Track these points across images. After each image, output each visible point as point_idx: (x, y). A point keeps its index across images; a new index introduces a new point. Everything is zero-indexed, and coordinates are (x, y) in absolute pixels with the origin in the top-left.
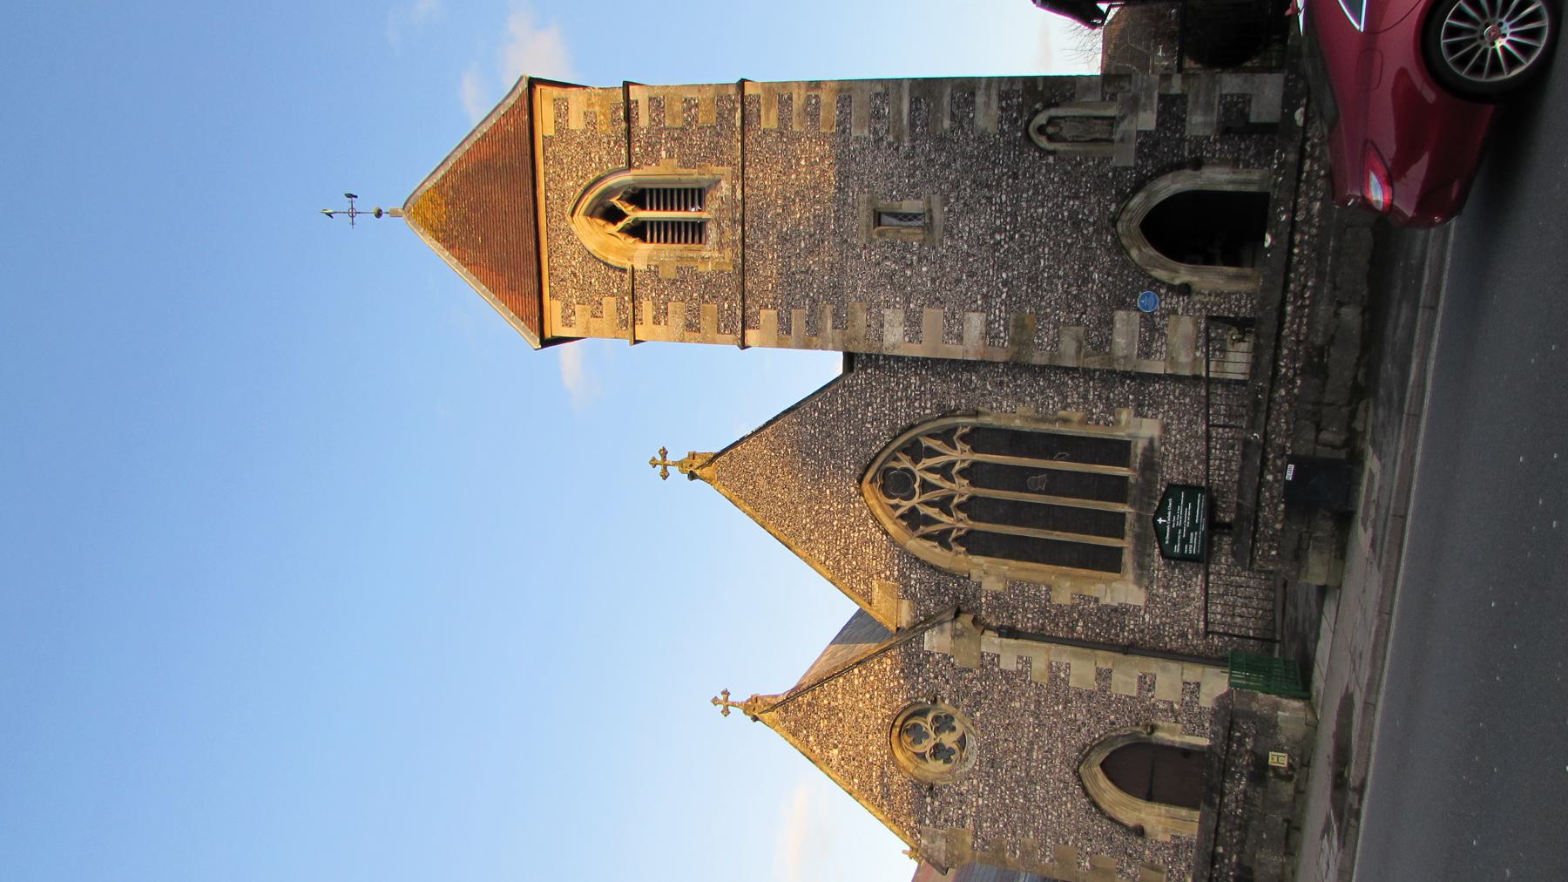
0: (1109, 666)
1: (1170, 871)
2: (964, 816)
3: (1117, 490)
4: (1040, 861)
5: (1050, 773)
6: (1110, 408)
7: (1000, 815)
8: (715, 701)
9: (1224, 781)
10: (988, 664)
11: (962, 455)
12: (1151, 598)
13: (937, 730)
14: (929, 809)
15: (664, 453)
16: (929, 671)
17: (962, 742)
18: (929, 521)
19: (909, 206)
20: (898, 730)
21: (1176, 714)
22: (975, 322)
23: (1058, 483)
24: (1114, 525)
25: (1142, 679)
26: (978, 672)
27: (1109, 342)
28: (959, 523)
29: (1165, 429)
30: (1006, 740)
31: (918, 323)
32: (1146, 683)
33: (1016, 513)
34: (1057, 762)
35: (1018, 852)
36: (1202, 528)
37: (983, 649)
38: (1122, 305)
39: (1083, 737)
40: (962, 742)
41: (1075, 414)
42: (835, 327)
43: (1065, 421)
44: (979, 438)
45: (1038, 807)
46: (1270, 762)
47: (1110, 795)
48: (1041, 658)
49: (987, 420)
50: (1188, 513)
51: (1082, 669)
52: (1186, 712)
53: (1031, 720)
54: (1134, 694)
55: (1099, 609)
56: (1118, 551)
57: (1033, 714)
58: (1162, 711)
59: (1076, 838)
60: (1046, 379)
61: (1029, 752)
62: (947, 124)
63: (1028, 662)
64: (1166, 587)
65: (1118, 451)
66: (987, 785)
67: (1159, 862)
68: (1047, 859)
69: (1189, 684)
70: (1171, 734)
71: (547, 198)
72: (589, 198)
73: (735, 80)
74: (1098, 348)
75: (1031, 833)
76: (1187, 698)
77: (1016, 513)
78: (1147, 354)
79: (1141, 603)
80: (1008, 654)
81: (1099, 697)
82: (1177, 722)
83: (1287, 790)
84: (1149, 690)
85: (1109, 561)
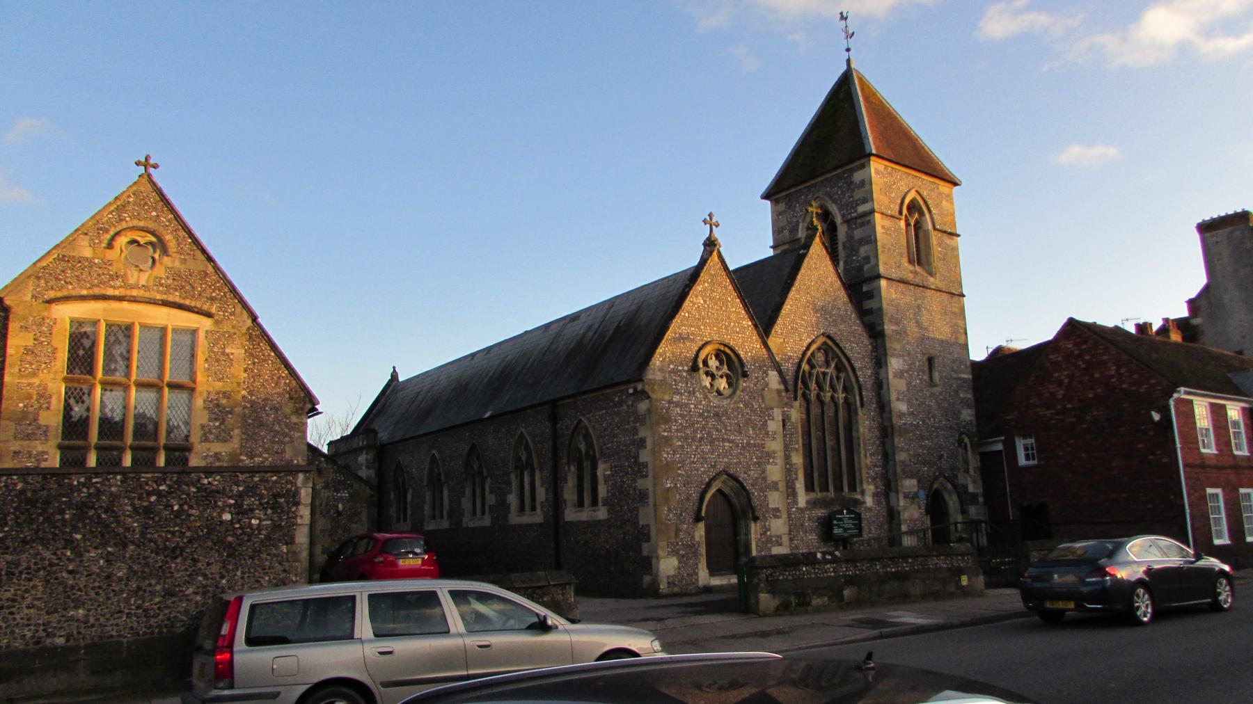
0: (781, 489)
1: (678, 544)
2: (681, 394)
3: (839, 488)
4: (664, 451)
5: (719, 456)
7: (687, 420)
8: (710, 215)
9: (943, 555)
10: (766, 413)
12: (802, 510)
14: (680, 368)
15: (155, 166)
16: (758, 373)
19: (936, 375)
20: (722, 349)
24: (825, 488)
25: (777, 510)
26: (763, 406)
27: (907, 477)
29: (870, 509)
34: (726, 460)
35: (666, 434)
36: (846, 535)
37: (775, 409)
38: (919, 482)
39: (742, 477)
41: (868, 461)
42: (892, 330)
43: (866, 456)
45: (697, 448)
46: (962, 576)
49: (860, 412)
50: (850, 526)
52: (768, 541)
53: (745, 441)
54: (770, 506)
55: (793, 480)
56: (827, 490)
57: (748, 444)
58: (765, 525)
59: (684, 475)
60: (879, 444)
61: (729, 441)
62: (962, 395)
63: (774, 438)
64: (809, 519)
66: (703, 412)
67: (682, 535)
68: (665, 455)
69: (781, 539)
70: (755, 529)
71: (899, 170)
72: (921, 202)
73: (964, 293)
74: (904, 472)
75: (680, 443)
76: (774, 539)
78: (906, 496)
82: (761, 534)
83: (952, 588)
84: (773, 515)
85: (809, 487)
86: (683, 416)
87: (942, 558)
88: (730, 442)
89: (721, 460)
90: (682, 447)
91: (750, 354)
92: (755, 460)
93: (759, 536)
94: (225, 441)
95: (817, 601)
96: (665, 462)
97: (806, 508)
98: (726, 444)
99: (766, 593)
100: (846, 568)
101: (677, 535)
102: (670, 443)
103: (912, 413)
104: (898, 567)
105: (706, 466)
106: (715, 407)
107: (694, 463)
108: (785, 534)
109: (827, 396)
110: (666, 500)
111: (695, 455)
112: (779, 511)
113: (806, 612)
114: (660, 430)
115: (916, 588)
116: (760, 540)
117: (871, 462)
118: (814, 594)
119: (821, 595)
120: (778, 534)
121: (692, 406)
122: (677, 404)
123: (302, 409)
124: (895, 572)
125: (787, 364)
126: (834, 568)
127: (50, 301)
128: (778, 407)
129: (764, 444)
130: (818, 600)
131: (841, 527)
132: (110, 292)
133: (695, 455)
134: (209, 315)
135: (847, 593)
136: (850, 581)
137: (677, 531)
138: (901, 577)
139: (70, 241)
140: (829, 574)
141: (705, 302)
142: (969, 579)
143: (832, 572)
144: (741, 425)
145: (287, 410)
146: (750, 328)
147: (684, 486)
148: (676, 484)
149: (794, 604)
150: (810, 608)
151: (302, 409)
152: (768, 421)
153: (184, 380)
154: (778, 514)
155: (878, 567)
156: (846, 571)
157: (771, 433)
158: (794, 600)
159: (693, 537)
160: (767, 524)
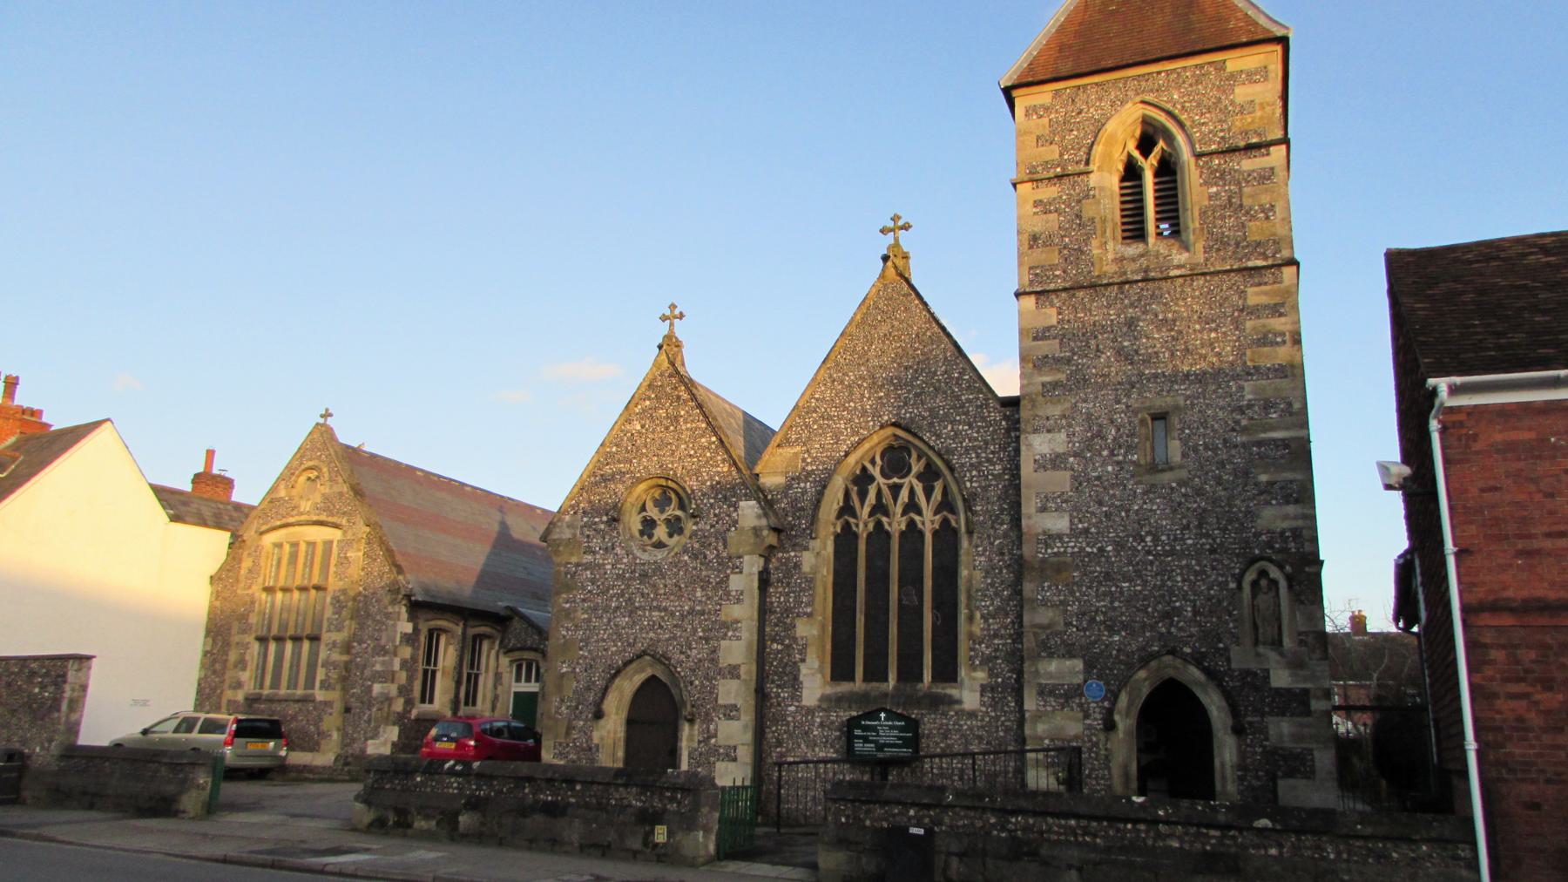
0: (743, 677)
1: (568, 745)
2: (594, 553)
3: (910, 672)
4: (562, 626)
6: (987, 661)
8: (673, 307)
10: (730, 564)
11: (928, 521)
12: (810, 711)
13: (668, 521)
14: (597, 520)
17: (660, 545)
18: (863, 495)
21: (706, 741)
22: (1059, 523)
23: (911, 616)
24: (876, 672)
25: (734, 707)
28: (863, 524)
29: (972, 715)
30: (665, 586)
31: (1055, 467)
32: (731, 712)
33: (878, 579)
34: (652, 635)
35: (568, 605)
36: (880, 755)
37: (746, 558)
40: (660, 545)
41: (978, 627)
44: (947, 537)
45: (609, 621)
47: (628, 685)
48: (744, 612)
49: (965, 543)
51: (737, 651)
53: (686, 608)
55: (795, 663)
58: (708, 728)
59: (586, 658)
63: (739, 601)
64: (822, 725)
65: (947, 671)
68: (564, 633)
69: (735, 751)
70: (688, 738)
73: (1297, 256)
75: (586, 616)
76: (721, 751)
77: (878, 579)
79: (804, 703)
80: (744, 581)
81: (715, 670)
82: (700, 742)
83: (636, 843)
84: (725, 715)
85: (841, 669)
86: (593, 581)
87: (634, 790)
88: (660, 610)
89: (644, 635)
90: (589, 620)
91: (709, 483)
92: (701, 634)
93: (696, 745)
94: (339, 630)
95: (420, 824)
96: (562, 641)
97: (819, 707)
98: (655, 613)
99: (362, 802)
100: (476, 784)
101: (568, 734)
102: (572, 616)
103: (1086, 531)
104: (558, 795)
105: (619, 644)
106: (644, 564)
107: (604, 640)
108: (743, 744)
109: (896, 524)
110: (560, 688)
111: (605, 630)
112: (738, 710)
113: (405, 836)
114: (561, 600)
115: (573, 831)
116: (696, 750)
117: (982, 629)
118: (419, 814)
119: (427, 817)
120: (732, 743)
121: (609, 567)
122: (588, 567)
123: (395, 599)
124: (551, 801)
125: (802, 485)
126: (459, 783)
127: (262, 533)
128: (751, 553)
129: (720, 610)
130: (423, 823)
131: (871, 742)
132: (291, 520)
133: (605, 630)
134: (336, 526)
135: (464, 819)
136: (474, 804)
137: (570, 729)
138: (552, 810)
139: (274, 489)
140: (451, 791)
141: (643, 426)
142: (670, 834)
143: (456, 788)
144: (683, 586)
145: (387, 600)
146: (713, 446)
147: (586, 671)
148: (574, 669)
149: (391, 823)
150: (410, 831)
151: (395, 599)
152: (732, 577)
153: (322, 583)
154: (734, 713)
155: (527, 791)
156: (476, 790)
157: (734, 593)
158: (392, 818)
159: (591, 738)
160: (712, 727)
